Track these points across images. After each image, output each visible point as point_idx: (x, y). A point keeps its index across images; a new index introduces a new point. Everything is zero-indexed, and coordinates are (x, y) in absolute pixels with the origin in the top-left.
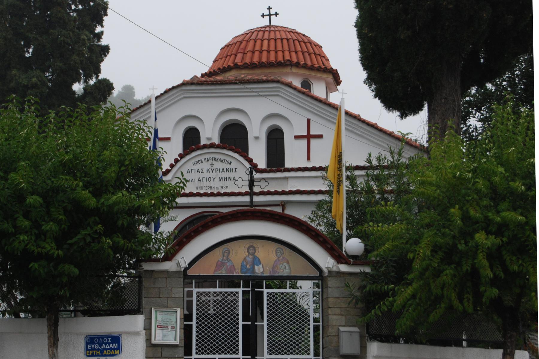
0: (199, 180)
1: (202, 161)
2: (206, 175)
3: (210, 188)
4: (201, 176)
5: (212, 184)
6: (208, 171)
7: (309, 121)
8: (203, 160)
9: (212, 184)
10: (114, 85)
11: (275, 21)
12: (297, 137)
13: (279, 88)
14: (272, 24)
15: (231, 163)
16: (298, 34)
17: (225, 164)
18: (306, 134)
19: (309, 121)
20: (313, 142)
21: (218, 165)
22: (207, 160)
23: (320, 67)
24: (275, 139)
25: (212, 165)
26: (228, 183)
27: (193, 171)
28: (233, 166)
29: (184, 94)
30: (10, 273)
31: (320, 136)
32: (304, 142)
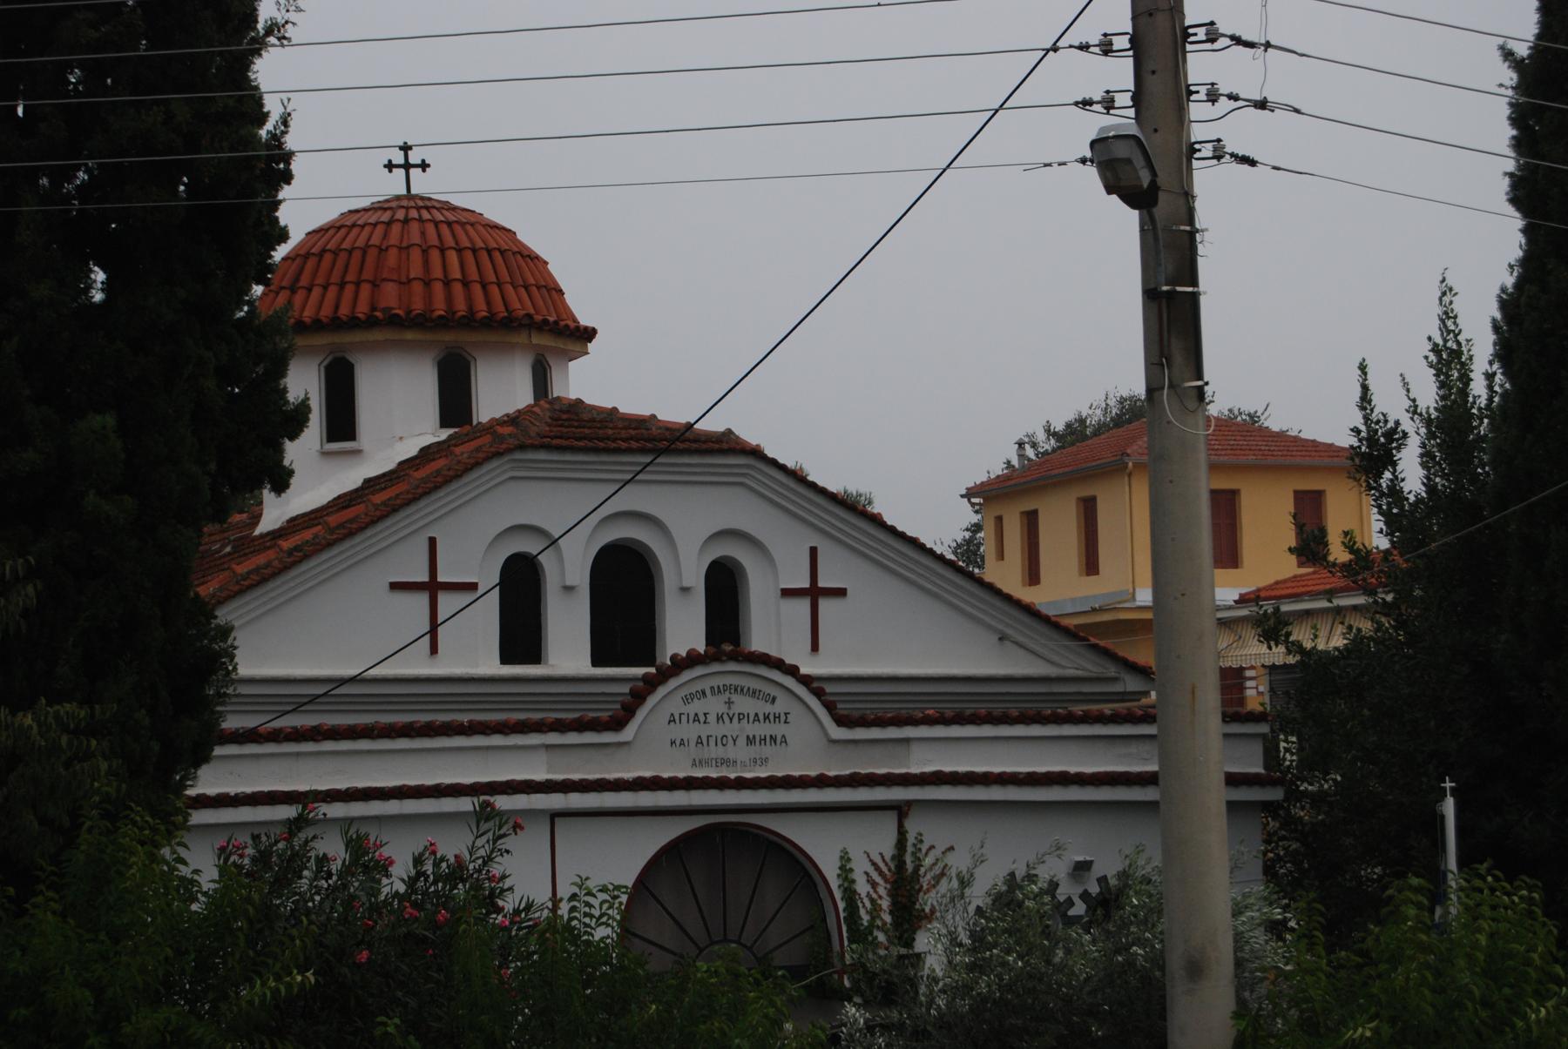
0: (699, 741)
1: (704, 693)
3: (725, 762)
4: (704, 730)
6: (720, 718)
7: (813, 551)
8: (708, 692)
9: (731, 752)
11: (422, 184)
12: (787, 593)
13: (748, 466)
14: (413, 192)
15: (774, 699)
17: (761, 703)
18: (807, 585)
19: (813, 551)
20: (825, 605)
21: (744, 704)
22: (717, 691)
23: (545, 322)
24: (724, 590)
25: (729, 703)
27: (684, 718)
28: (779, 707)
29: (512, 469)
30: (524, 1015)
31: (840, 593)
32: (804, 605)
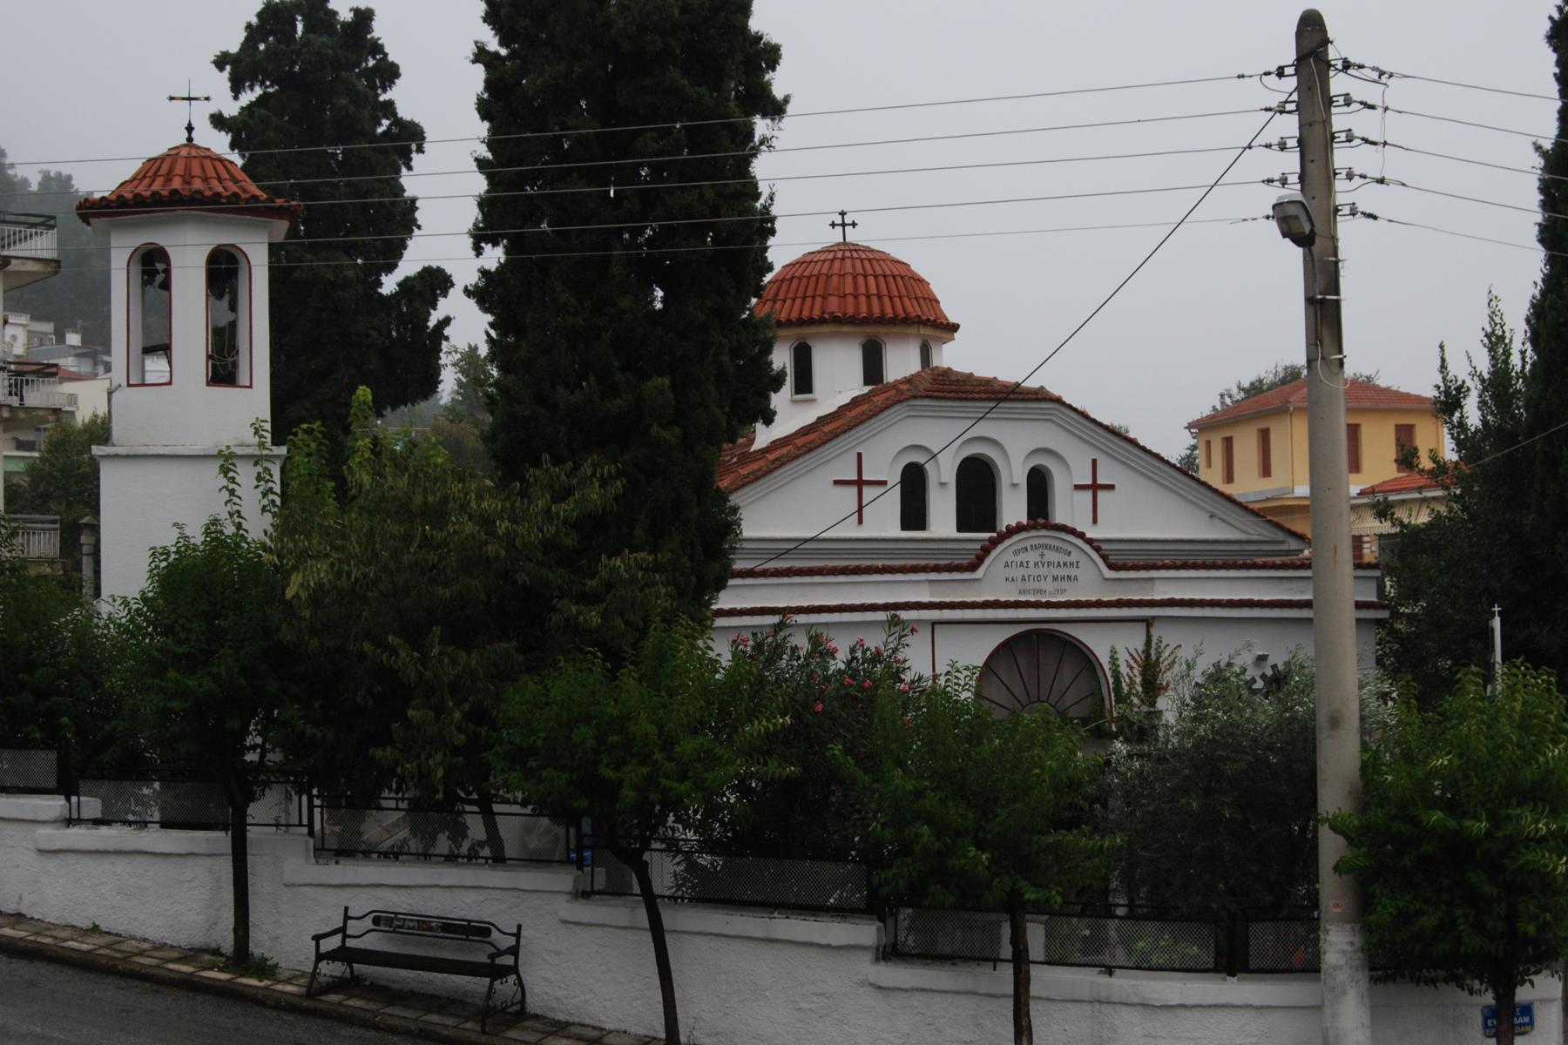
0: (1023, 579)
2: (1033, 571)
3: (1039, 591)
4: (1026, 572)
5: (1042, 585)
6: (1036, 564)
7: (1094, 462)
9: (1042, 585)
10: (454, 279)
11: (853, 236)
12: (1078, 487)
16: (872, 251)
19: (1094, 462)
20: (1101, 494)
21: (1051, 556)
24: (1039, 484)
26: (1065, 585)
28: (1074, 557)
31: (1111, 487)
32: (1088, 495)
